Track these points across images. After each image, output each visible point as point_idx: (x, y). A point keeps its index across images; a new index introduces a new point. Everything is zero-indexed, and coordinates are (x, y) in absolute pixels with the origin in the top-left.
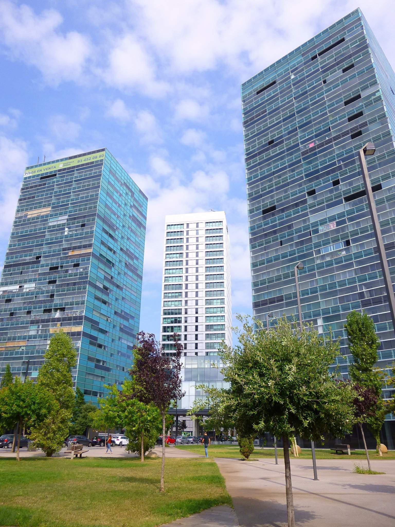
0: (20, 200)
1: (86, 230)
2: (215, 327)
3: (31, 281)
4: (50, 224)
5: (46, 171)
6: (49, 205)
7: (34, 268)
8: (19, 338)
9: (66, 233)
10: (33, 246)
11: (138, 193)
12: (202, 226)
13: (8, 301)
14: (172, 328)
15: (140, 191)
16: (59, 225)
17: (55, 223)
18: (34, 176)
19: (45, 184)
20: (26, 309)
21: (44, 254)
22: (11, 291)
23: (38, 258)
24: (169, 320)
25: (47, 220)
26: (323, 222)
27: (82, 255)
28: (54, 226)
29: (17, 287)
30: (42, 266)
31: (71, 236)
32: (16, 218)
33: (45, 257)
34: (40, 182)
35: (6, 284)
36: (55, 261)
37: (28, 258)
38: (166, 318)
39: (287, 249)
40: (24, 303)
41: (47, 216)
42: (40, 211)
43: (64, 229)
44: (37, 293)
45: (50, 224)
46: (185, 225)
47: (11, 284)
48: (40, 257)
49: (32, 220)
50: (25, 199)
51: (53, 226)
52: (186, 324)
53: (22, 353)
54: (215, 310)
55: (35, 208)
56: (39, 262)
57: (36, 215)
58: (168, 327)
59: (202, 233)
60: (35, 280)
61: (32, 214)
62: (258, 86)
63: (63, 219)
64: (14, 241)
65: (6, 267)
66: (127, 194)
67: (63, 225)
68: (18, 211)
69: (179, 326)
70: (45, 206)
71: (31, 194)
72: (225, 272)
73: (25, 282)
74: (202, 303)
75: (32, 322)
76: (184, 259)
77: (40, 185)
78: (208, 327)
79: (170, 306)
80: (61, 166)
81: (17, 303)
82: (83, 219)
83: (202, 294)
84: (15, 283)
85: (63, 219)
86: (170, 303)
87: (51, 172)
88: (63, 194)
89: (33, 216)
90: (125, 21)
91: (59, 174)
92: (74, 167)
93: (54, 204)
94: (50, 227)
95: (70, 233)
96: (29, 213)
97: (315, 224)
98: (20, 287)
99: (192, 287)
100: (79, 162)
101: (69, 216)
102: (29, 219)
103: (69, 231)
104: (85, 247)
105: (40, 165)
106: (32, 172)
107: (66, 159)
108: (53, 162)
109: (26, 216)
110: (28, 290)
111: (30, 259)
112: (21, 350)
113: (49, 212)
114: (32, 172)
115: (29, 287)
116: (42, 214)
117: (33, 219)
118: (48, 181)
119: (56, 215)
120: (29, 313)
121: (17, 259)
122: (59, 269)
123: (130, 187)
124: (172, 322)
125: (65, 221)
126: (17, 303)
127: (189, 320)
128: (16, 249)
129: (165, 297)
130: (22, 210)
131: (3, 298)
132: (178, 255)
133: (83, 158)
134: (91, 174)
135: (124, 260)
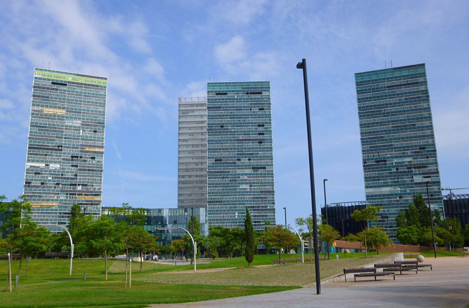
1: (98, 135)
4: (66, 124)
22: (39, 167)
26: (242, 175)
36: (76, 152)
39: (224, 181)
43: (80, 130)
62: (217, 89)
73: (51, 162)
85: (78, 123)
97: (239, 174)
133: (90, 79)
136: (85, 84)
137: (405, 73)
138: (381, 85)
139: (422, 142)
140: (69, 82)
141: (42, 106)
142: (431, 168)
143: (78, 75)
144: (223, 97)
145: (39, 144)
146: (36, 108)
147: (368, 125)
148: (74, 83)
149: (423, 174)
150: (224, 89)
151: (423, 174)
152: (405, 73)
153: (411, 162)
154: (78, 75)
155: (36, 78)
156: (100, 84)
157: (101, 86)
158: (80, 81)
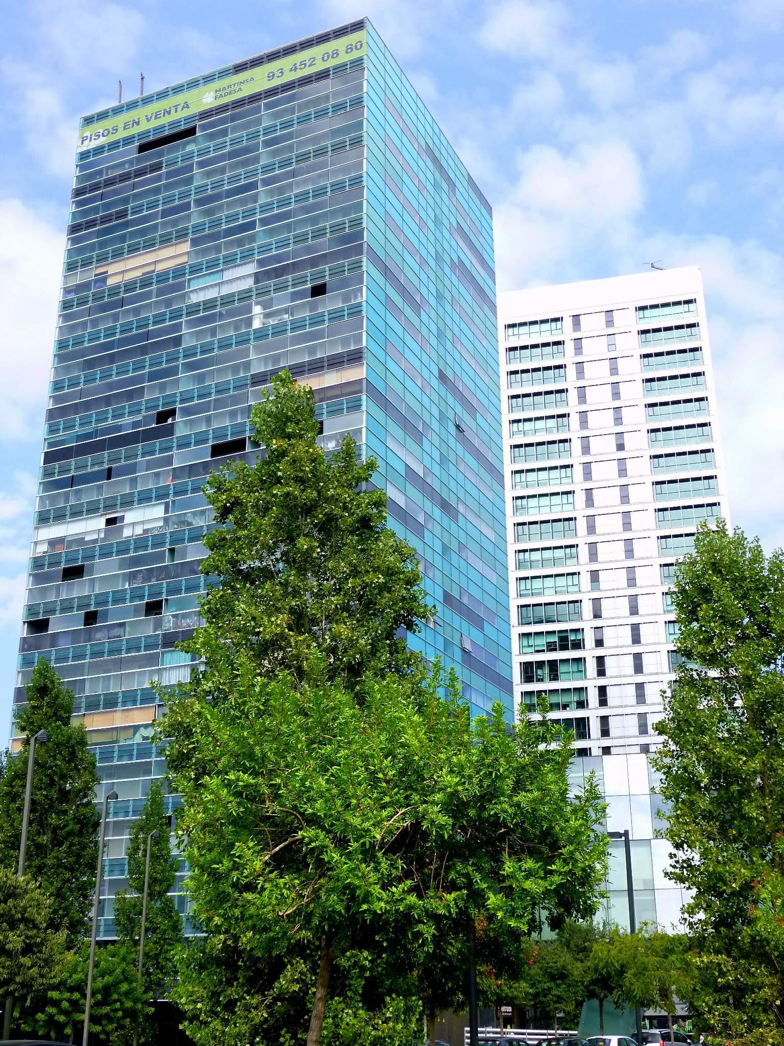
0: (74, 229)
1: (329, 303)
3: (149, 499)
5: (154, 124)
6: (182, 235)
7: (152, 453)
8: (130, 698)
9: (257, 324)
10: (140, 379)
11: (465, 184)
12: (628, 321)
13: (73, 573)
14: (553, 665)
15: (470, 180)
16: (227, 300)
17: (212, 294)
18: (113, 145)
19: (158, 167)
20: (142, 597)
21: (183, 401)
22: (81, 541)
23: (162, 417)
24: (541, 642)
25: (180, 287)
27: (329, 394)
28: (209, 304)
29: (100, 523)
30: (184, 444)
31: (279, 330)
32: (67, 291)
33: (187, 412)
34: (138, 160)
35: (60, 517)
37: (127, 420)
38: (528, 635)
40: (132, 577)
41: (179, 272)
42: (149, 258)
44: (177, 539)
45: (195, 299)
46: (568, 323)
47: (76, 513)
48: (172, 413)
49: (126, 291)
50: (91, 224)
51: (205, 302)
52: (600, 652)
53: (144, 752)
55: (129, 252)
56: (170, 430)
57: (138, 273)
58: (540, 664)
59: (630, 346)
60: (161, 495)
61: (123, 270)
63: (240, 277)
64: (68, 369)
65: (50, 458)
66: (436, 186)
67: (245, 296)
68: (71, 267)
69: (578, 660)
70: (166, 241)
71: (107, 207)
72: (722, 464)
73: (127, 503)
75: (169, 641)
76: (574, 432)
77: (139, 173)
79: (539, 594)
80: (208, 98)
81: (106, 575)
82: (324, 263)
84: (89, 511)
86: (537, 584)
88: (230, 193)
89: (129, 276)
91: (204, 127)
92: (255, 98)
93: (198, 228)
94: (194, 309)
95: (272, 321)
96: (112, 269)
98: (110, 522)
99: (609, 525)
100: (271, 76)
101: (261, 263)
102: (114, 290)
103: (267, 316)
104: (336, 362)
105: (132, 105)
106: (107, 133)
107: (223, 74)
108: (178, 90)
109: (102, 279)
110: (139, 530)
111: (136, 424)
112: (138, 739)
113: (184, 259)
114: (107, 133)
115: (142, 519)
116: (160, 267)
117: (130, 286)
118: (171, 155)
119: (213, 264)
120: (154, 608)
121: (88, 429)
122: (248, 449)
123: (443, 163)
124: (551, 647)
125: (249, 283)
126: (106, 575)
127: (609, 636)
128: (81, 394)
129: (520, 565)
130: (86, 263)
131: (51, 565)
132: (551, 423)
134: (220, 184)
135: (451, 415)
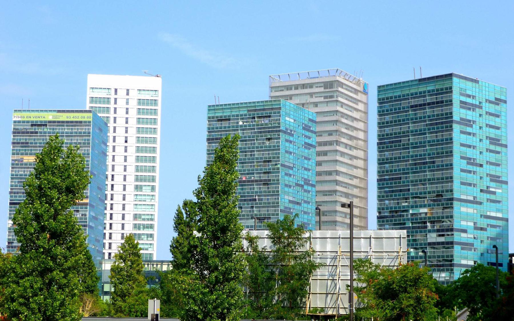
2: (143, 217)
54: (143, 197)
59: (133, 105)
74: (130, 189)
78: (136, 217)
83: (131, 179)
87: (41, 121)
90: (182, 318)
106: (21, 117)
133: (72, 115)
136: (67, 122)
137: (431, 87)
138: (405, 104)
139: (439, 187)
140: (50, 122)
141: (22, 154)
142: (446, 224)
143: (59, 111)
144: (225, 124)
145: (20, 198)
146: (16, 157)
147: (389, 161)
148: (54, 122)
149: (438, 231)
150: (227, 113)
151: (438, 231)
152: (431, 87)
153: (426, 213)
154: (59, 111)
155: (15, 122)
156: (83, 120)
157: (85, 122)
158: (61, 119)
